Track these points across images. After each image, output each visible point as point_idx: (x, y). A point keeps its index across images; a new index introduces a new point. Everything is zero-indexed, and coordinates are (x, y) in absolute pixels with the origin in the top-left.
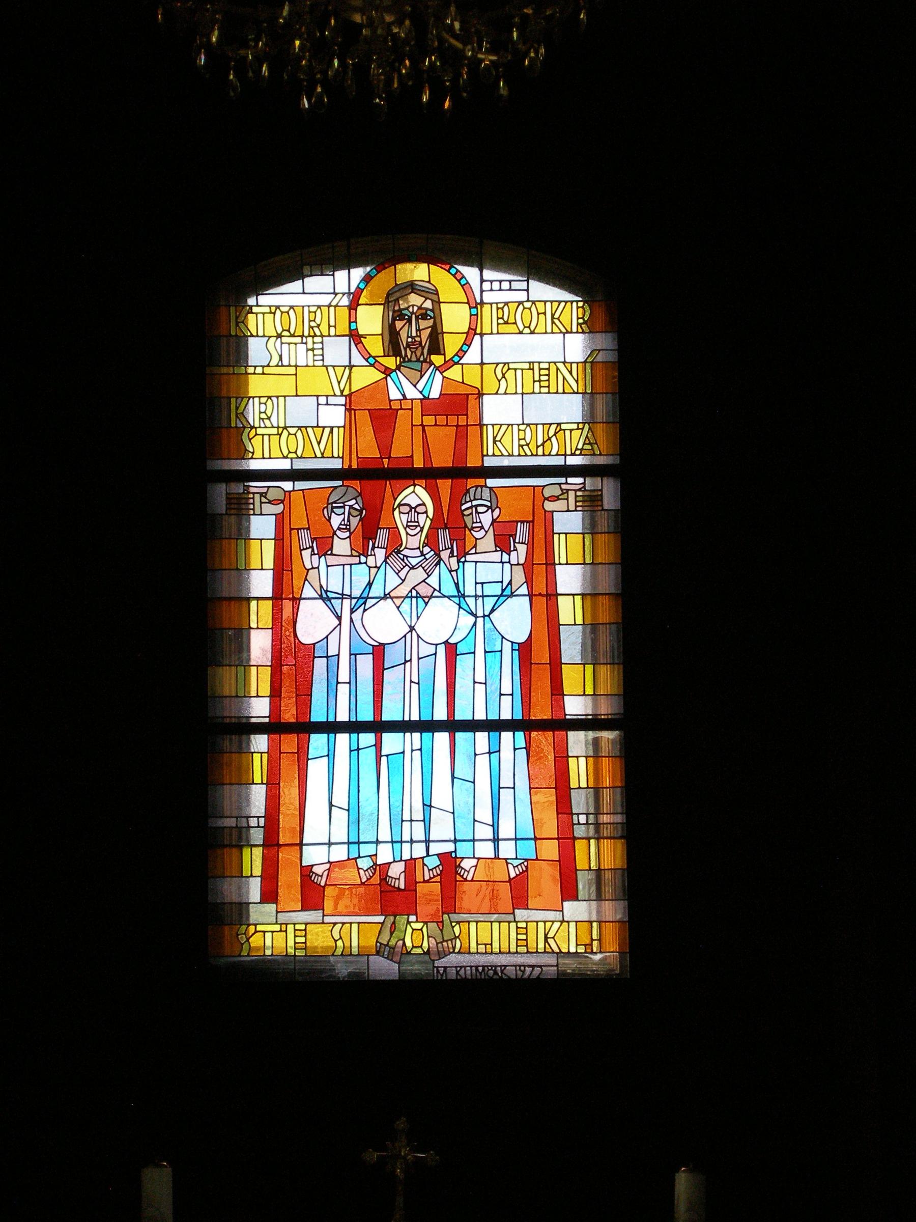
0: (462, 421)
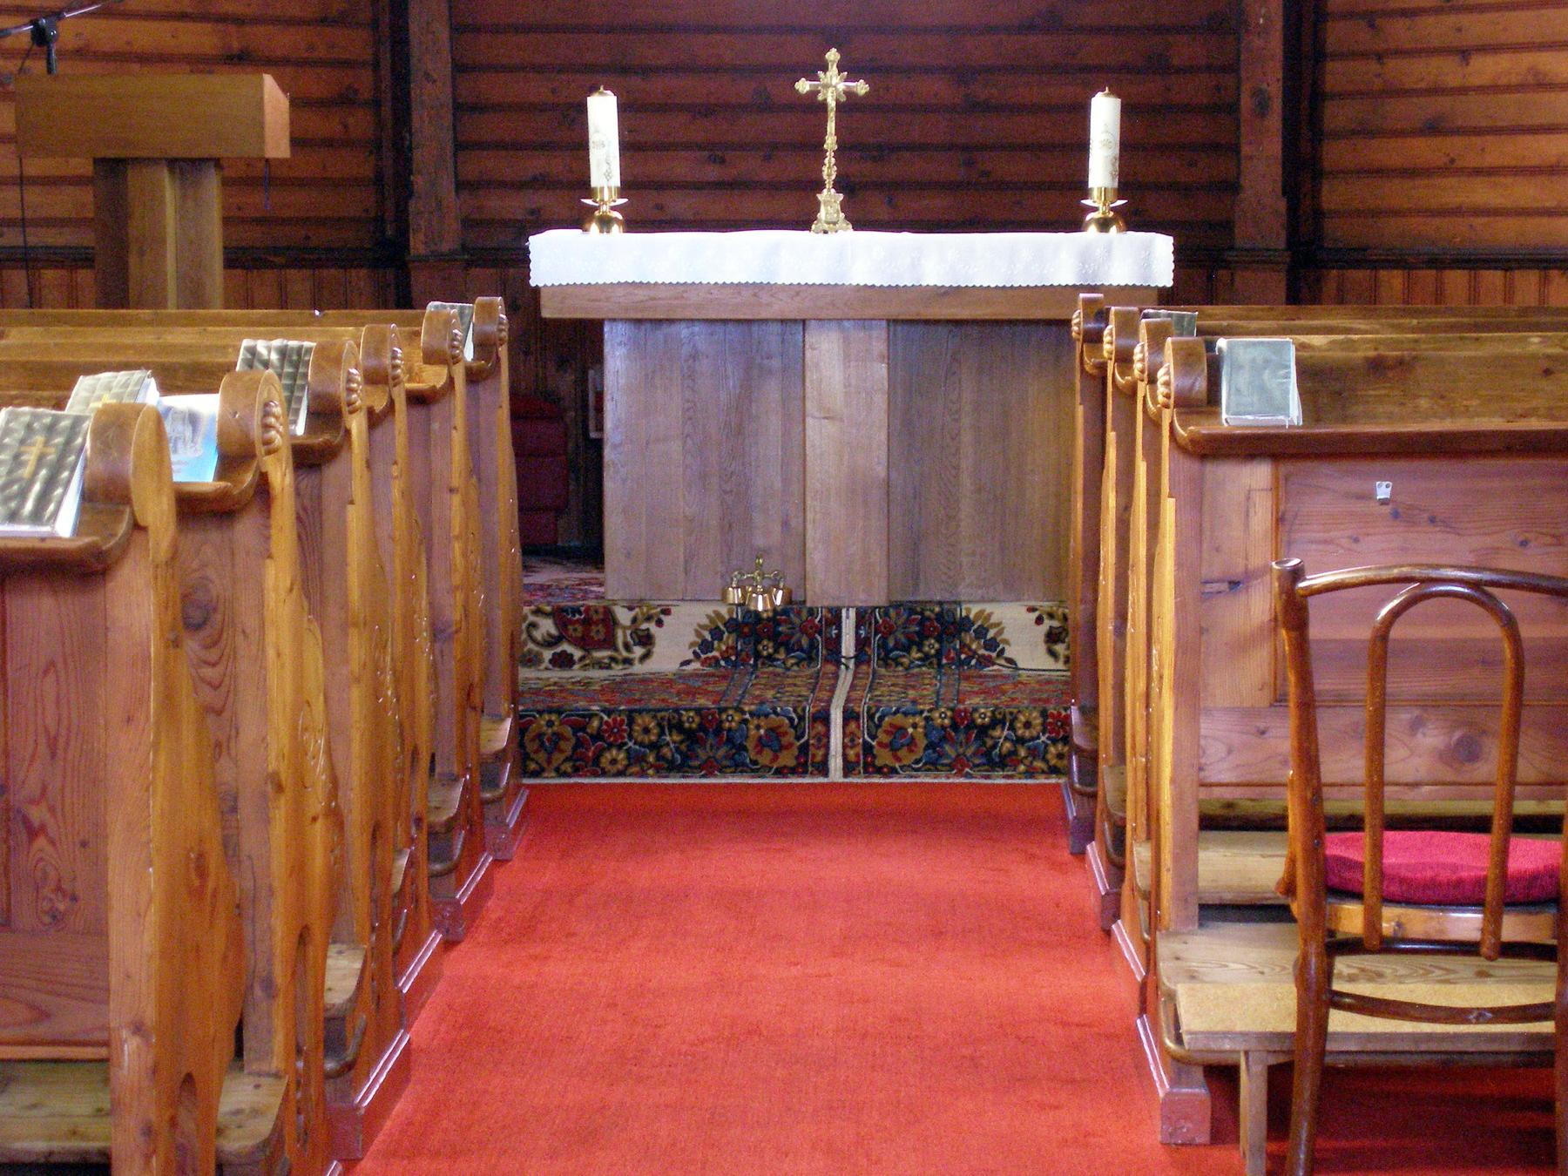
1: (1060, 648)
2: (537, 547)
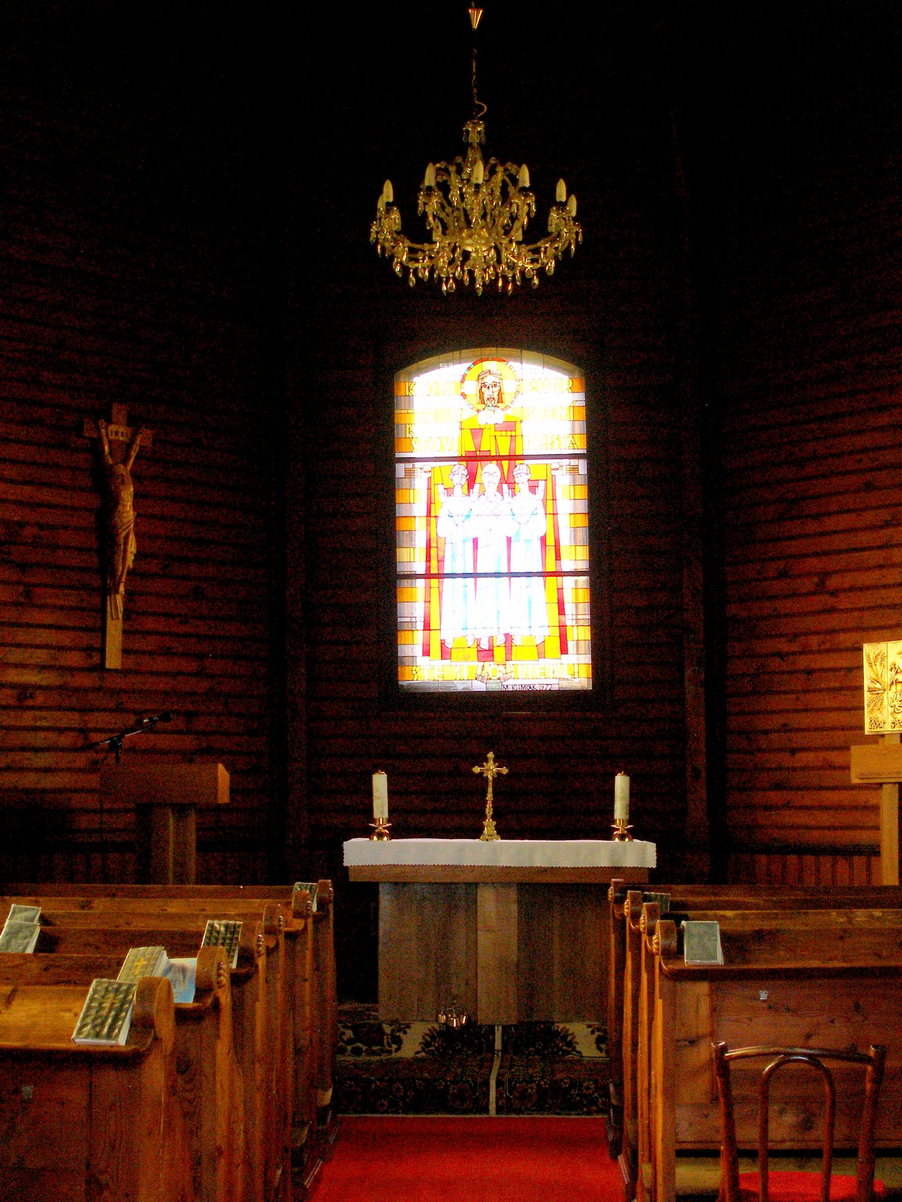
0: (513, 434)
1: (603, 1046)
2: (344, 992)
